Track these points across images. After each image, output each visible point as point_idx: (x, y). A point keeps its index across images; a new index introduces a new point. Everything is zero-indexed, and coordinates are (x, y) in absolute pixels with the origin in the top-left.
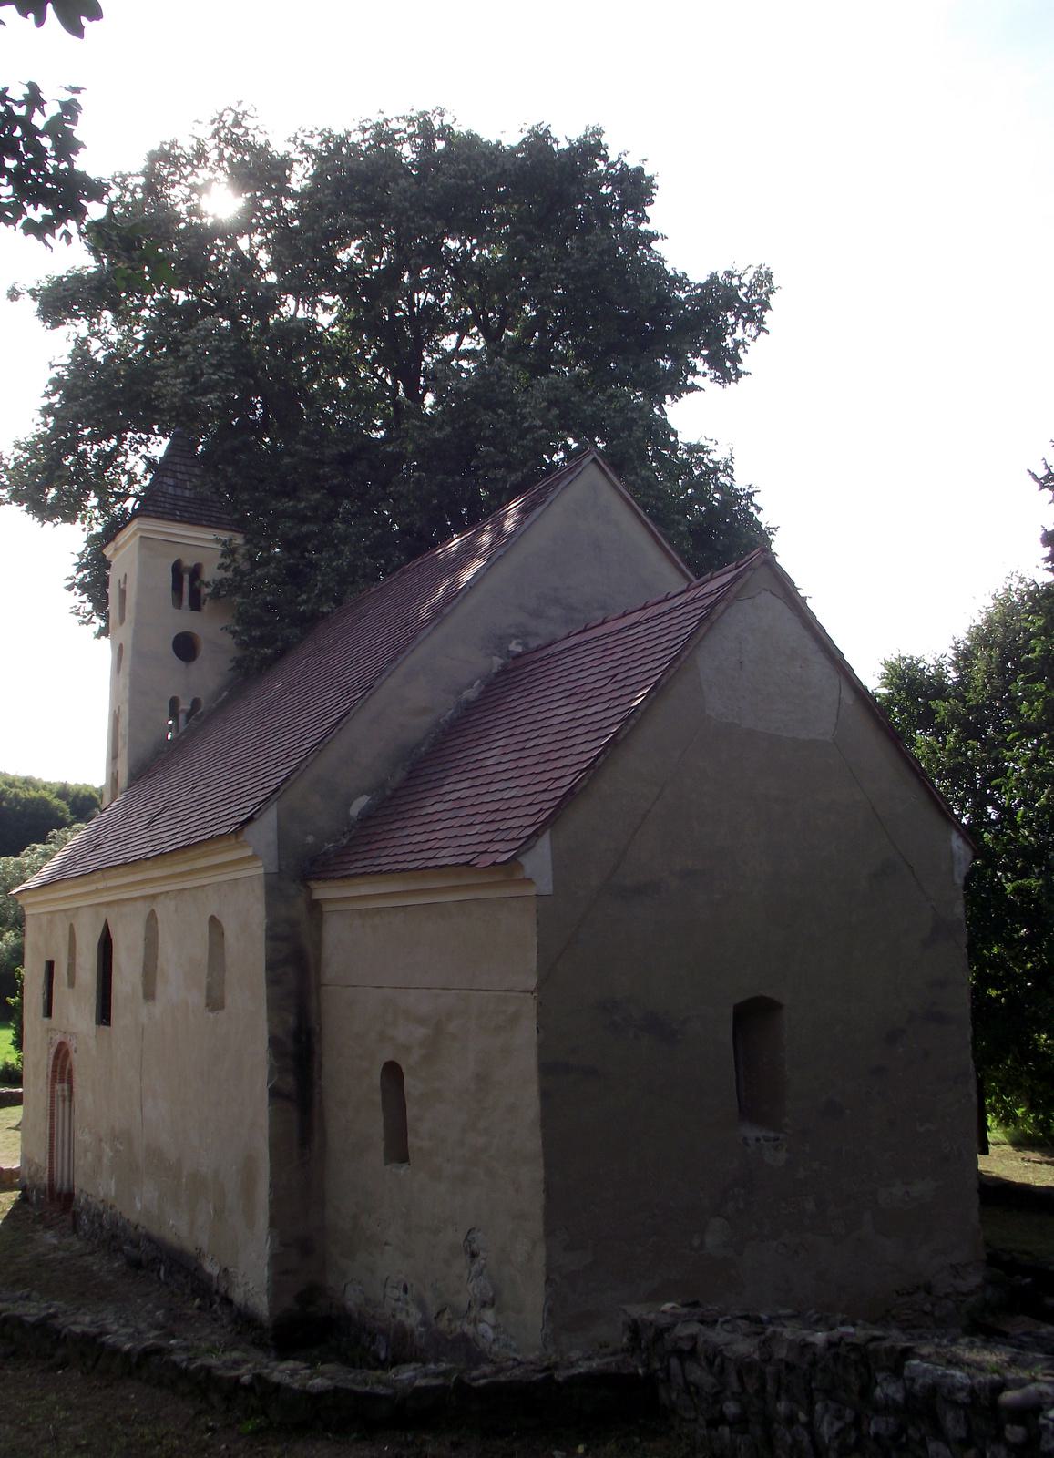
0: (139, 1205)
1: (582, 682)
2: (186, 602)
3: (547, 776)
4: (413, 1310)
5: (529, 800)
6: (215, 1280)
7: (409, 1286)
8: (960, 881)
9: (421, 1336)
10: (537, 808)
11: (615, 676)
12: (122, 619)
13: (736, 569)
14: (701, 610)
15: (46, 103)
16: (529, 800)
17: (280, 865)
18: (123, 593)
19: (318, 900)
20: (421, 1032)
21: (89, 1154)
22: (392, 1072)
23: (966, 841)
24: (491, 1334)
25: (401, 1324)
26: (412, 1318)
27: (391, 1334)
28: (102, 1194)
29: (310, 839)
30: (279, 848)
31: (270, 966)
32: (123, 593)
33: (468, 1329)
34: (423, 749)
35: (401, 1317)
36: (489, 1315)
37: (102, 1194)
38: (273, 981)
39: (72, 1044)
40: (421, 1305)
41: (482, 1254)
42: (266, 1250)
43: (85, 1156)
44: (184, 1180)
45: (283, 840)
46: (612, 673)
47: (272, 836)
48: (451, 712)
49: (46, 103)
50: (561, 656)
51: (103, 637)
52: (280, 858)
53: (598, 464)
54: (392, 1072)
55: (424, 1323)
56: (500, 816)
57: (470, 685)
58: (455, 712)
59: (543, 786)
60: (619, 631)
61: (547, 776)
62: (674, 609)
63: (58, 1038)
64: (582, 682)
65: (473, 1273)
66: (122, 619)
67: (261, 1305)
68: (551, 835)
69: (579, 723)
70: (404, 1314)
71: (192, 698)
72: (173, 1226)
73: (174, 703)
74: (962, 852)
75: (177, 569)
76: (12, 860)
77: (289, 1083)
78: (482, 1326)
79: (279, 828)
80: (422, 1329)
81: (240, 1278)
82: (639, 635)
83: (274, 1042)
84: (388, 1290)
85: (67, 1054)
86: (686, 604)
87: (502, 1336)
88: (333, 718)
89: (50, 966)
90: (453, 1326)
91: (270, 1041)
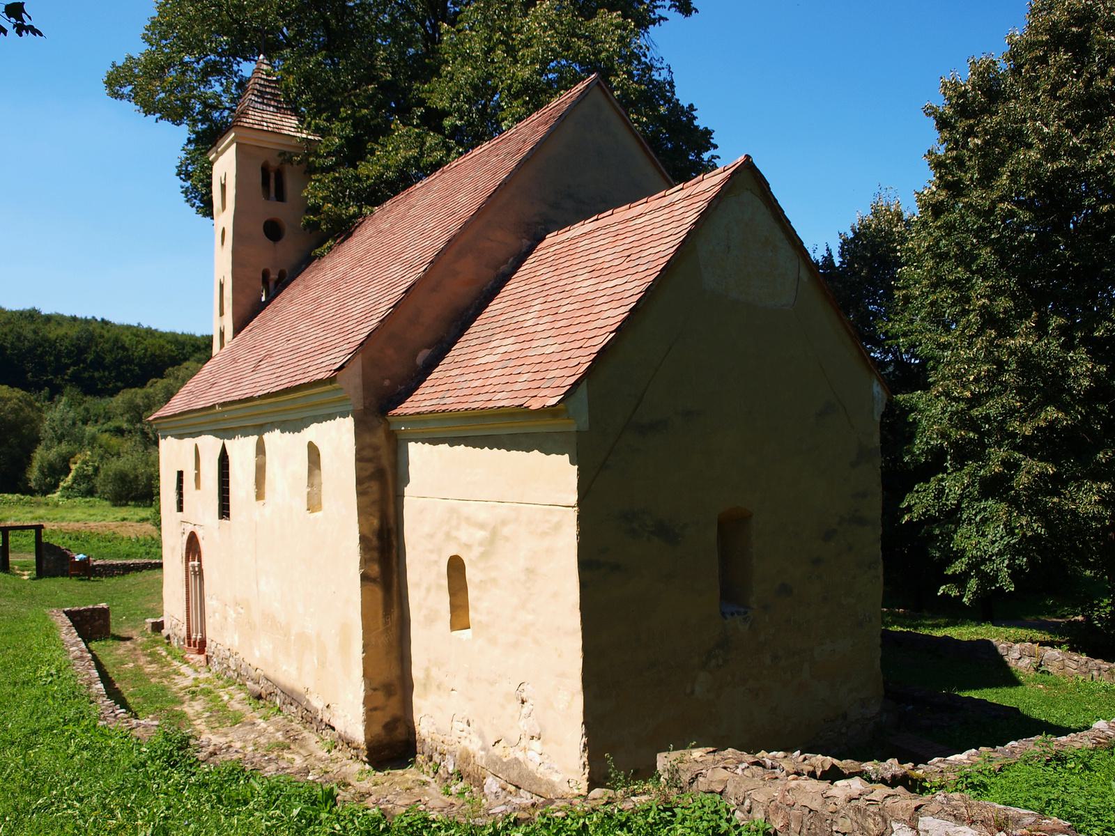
0: (257, 654)
1: (601, 260)
2: (272, 194)
3: (580, 336)
4: (475, 738)
5: (567, 355)
6: (320, 712)
7: (471, 721)
8: (878, 419)
9: (482, 757)
10: (575, 362)
11: (629, 256)
12: (224, 207)
13: (724, 171)
14: (702, 203)
15: (23, 3)
16: (567, 355)
17: (364, 403)
18: (223, 187)
19: (393, 431)
20: (481, 534)
21: (217, 614)
22: (456, 567)
23: (883, 388)
24: (538, 759)
25: (465, 749)
26: (473, 745)
27: (458, 754)
28: (228, 643)
29: (387, 383)
30: (364, 389)
31: (360, 481)
32: (223, 187)
33: (520, 755)
34: (471, 312)
35: (465, 743)
36: (536, 744)
37: (228, 643)
38: (360, 493)
39: (200, 534)
40: (482, 736)
41: (530, 701)
42: (361, 694)
43: (214, 616)
44: (293, 638)
45: (367, 384)
46: (627, 253)
47: (358, 381)
48: (491, 283)
49: (23, 3)
50: (580, 239)
51: (933, 122)
52: (365, 398)
53: (602, 87)
54: (456, 567)
55: (483, 749)
56: (543, 367)
57: (506, 262)
58: (495, 282)
59: (578, 344)
60: (627, 220)
61: (580, 336)
62: (673, 204)
63: (189, 528)
64: (601, 260)
65: (523, 715)
66: (224, 207)
67: (358, 733)
68: (587, 382)
69: (602, 293)
70: (468, 740)
71: (279, 270)
72: (285, 671)
73: (265, 275)
74: (880, 396)
75: (265, 170)
76: (140, 392)
77: (375, 570)
78: (530, 754)
79: (364, 374)
80: (483, 753)
81: (340, 711)
82: (647, 223)
83: (363, 539)
84: (455, 723)
85: (197, 542)
86: (684, 199)
87: (547, 761)
88: (401, 288)
89: (180, 474)
90: (507, 752)
91: (360, 538)
